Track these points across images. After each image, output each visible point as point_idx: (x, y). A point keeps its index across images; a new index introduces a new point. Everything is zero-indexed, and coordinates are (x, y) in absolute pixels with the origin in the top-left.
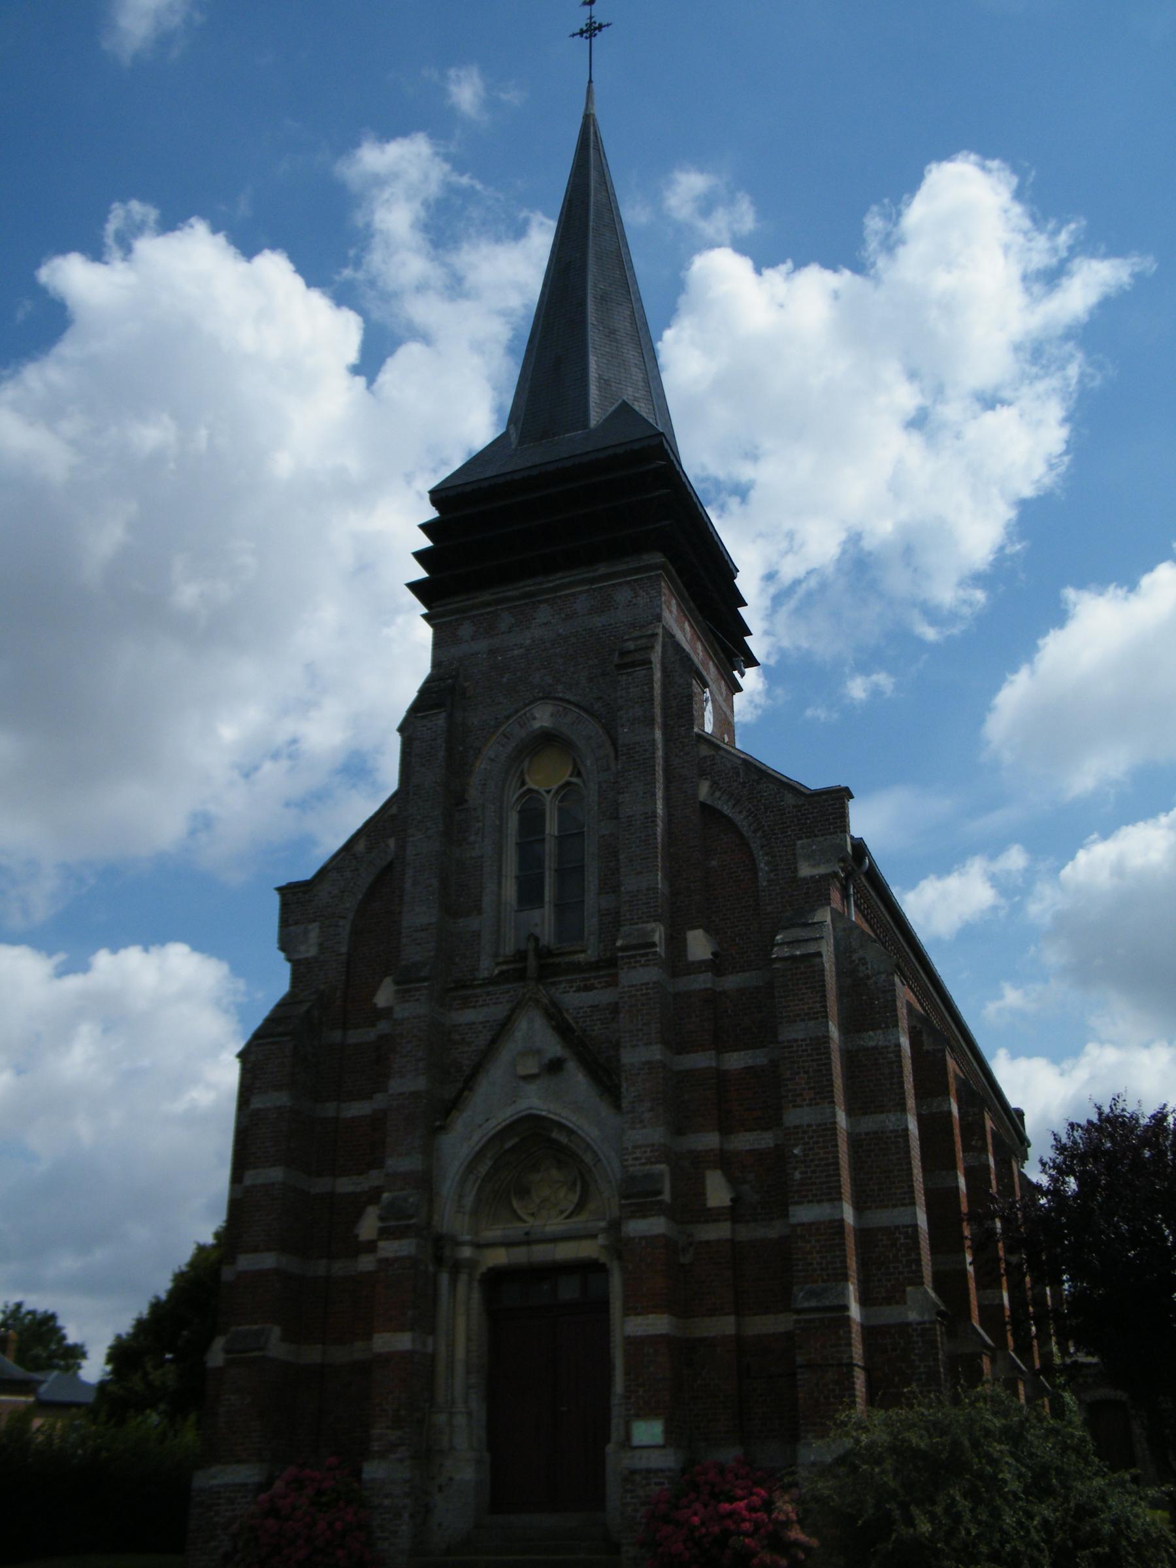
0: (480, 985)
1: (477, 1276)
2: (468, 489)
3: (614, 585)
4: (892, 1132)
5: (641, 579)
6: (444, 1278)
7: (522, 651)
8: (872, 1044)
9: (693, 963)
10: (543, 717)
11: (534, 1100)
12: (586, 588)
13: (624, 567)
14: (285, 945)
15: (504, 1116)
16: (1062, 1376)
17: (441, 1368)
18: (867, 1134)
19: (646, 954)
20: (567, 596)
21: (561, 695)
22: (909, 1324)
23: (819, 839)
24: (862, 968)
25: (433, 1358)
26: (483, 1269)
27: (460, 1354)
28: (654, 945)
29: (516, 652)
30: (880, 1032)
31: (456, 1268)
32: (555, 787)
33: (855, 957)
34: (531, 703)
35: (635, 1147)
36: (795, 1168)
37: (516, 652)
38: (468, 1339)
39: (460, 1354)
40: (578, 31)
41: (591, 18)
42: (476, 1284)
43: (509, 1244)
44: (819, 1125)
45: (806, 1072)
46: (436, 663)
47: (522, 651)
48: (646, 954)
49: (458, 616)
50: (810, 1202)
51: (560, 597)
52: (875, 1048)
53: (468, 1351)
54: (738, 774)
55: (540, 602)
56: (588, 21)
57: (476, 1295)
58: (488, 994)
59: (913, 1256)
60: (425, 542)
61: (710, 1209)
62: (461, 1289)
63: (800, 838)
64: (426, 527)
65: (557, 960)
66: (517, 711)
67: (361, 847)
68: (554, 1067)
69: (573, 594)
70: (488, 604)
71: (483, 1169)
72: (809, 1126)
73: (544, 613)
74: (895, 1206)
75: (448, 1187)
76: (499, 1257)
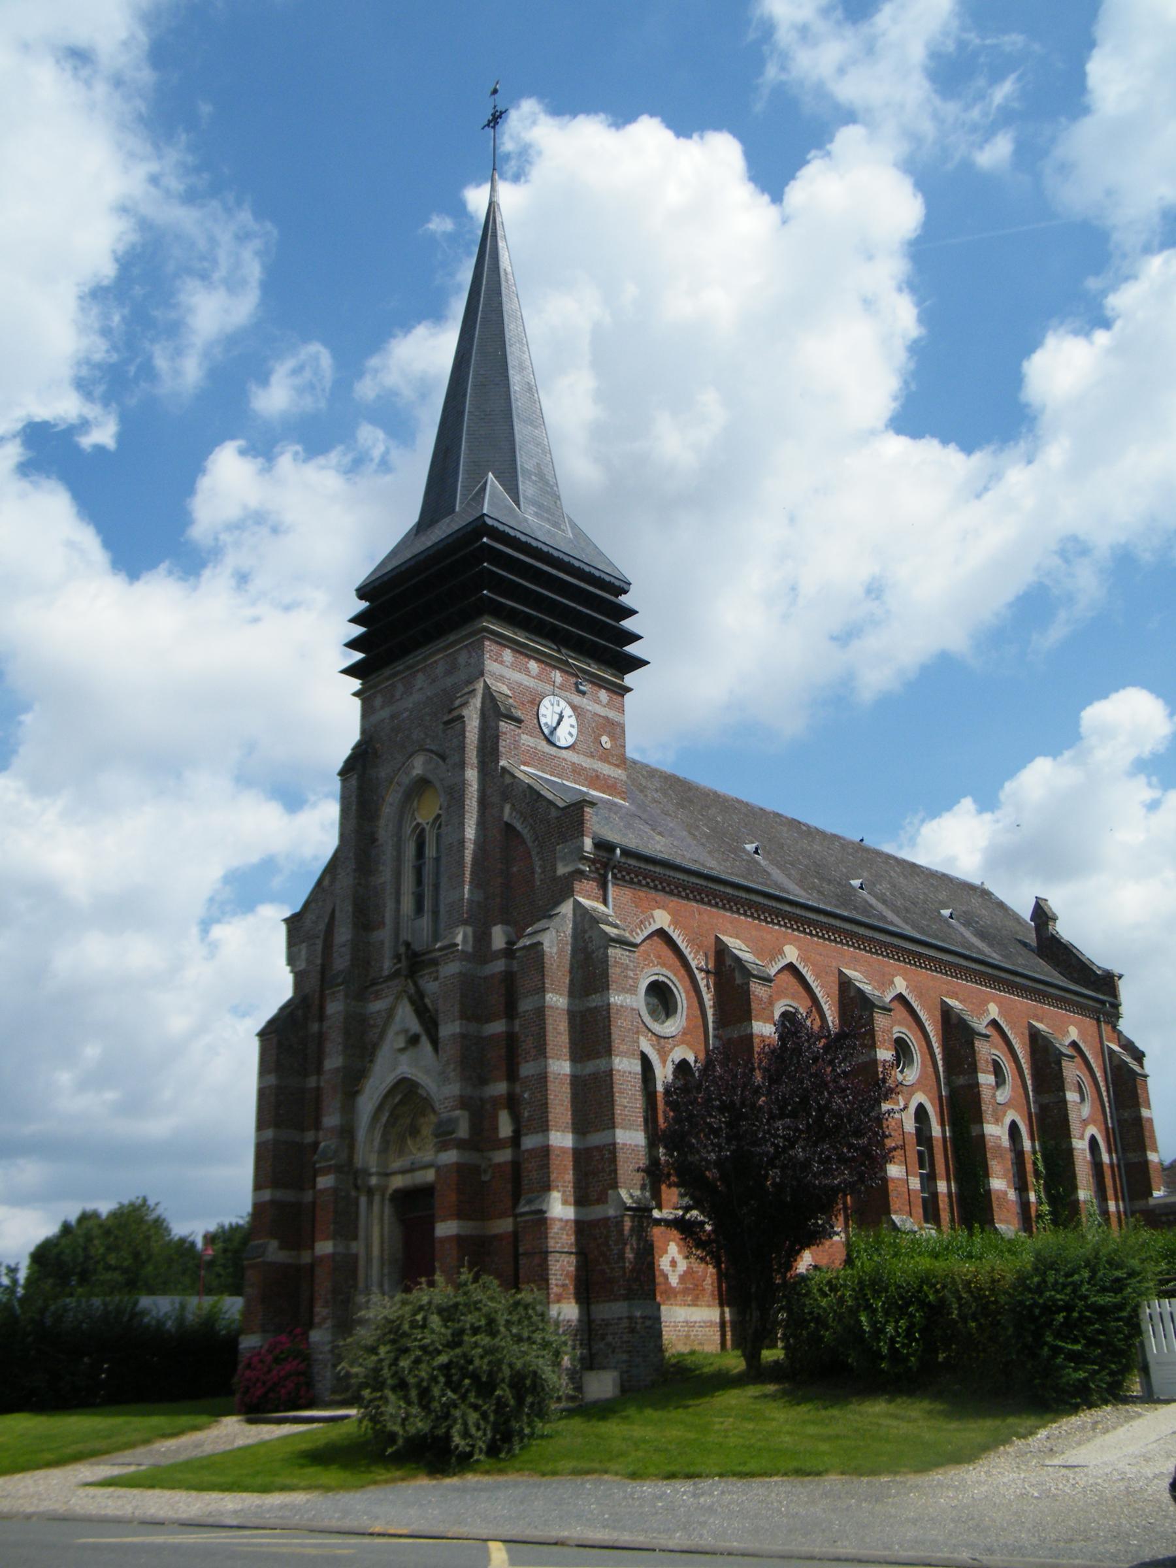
0: (384, 982)
1: (387, 1196)
2: (385, 579)
3: (458, 650)
4: (604, 1072)
5: (473, 642)
6: (363, 1200)
7: (408, 713)
8: (594, 1005)
9: (495, 952)
10: (418, 766)
11: (406, 1067)
12: (441, 655)
13: (464, 633)
14: (291, 960)
15: (390, 1079)
16: (1120, 1236)
17: (362, 1263)
18: (589, 1075)
19: (453, 953)
20: (431, 664)
21: (427, 747)
22: (608, 1218)
23: (570, 843)
24: (590, 945)
25: (356, 1256)
26: (390, 1191)
27: (376, 1251)
28: (458, 945)
29: (405, 715)
30: (598, 995)
31: (370, 1192)
32: (431, 820)
33: (587, 936)
34: (410, 757)
35: (446, 1099)
36: (525, 1109)
37: (405, 715)
38: (382, 1243)
39: (376, 1251)
40: (486, 123)
41: (495, 107)
42: (387, 1202)
43: (403, 1172)
44: (538, 1075)
45: (532, 1035)
46: (364, 731)
47: (408, 713)
48: (453, 953)
49: (372, 692)
50: (532, 1133)
51: (428, 665)
52: (596, 1008)
53: (382, 1250)
54: (525, 795)
55: (418, 671)
56: (493, 111)
57: (387, 1211)
58: (388, 987)
59: (612, 1168)
60: (358, 630)
61: (501, 1139)
62: (376, 1207)
63: (558, 844)
64: (356, 620)
65: (423, 958)
66: (404, 764)
67: (326, 882)
68: (414, 1040)
69: (435, 662)
70: (387, 679)
71: (384, 1118)
72: (533, 1076)
73: (420, 680)
74: (604, 1129)
75: (361, 1134)
76: (398, 1182)
